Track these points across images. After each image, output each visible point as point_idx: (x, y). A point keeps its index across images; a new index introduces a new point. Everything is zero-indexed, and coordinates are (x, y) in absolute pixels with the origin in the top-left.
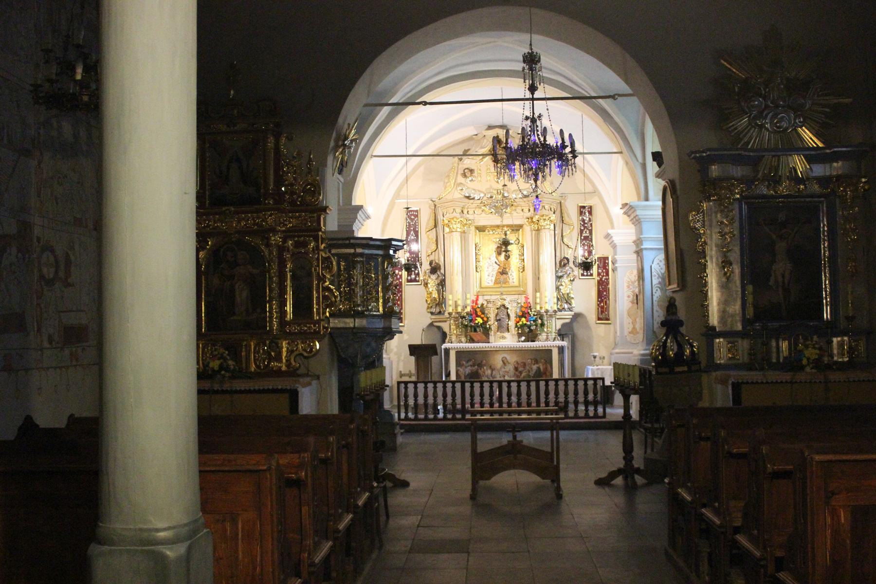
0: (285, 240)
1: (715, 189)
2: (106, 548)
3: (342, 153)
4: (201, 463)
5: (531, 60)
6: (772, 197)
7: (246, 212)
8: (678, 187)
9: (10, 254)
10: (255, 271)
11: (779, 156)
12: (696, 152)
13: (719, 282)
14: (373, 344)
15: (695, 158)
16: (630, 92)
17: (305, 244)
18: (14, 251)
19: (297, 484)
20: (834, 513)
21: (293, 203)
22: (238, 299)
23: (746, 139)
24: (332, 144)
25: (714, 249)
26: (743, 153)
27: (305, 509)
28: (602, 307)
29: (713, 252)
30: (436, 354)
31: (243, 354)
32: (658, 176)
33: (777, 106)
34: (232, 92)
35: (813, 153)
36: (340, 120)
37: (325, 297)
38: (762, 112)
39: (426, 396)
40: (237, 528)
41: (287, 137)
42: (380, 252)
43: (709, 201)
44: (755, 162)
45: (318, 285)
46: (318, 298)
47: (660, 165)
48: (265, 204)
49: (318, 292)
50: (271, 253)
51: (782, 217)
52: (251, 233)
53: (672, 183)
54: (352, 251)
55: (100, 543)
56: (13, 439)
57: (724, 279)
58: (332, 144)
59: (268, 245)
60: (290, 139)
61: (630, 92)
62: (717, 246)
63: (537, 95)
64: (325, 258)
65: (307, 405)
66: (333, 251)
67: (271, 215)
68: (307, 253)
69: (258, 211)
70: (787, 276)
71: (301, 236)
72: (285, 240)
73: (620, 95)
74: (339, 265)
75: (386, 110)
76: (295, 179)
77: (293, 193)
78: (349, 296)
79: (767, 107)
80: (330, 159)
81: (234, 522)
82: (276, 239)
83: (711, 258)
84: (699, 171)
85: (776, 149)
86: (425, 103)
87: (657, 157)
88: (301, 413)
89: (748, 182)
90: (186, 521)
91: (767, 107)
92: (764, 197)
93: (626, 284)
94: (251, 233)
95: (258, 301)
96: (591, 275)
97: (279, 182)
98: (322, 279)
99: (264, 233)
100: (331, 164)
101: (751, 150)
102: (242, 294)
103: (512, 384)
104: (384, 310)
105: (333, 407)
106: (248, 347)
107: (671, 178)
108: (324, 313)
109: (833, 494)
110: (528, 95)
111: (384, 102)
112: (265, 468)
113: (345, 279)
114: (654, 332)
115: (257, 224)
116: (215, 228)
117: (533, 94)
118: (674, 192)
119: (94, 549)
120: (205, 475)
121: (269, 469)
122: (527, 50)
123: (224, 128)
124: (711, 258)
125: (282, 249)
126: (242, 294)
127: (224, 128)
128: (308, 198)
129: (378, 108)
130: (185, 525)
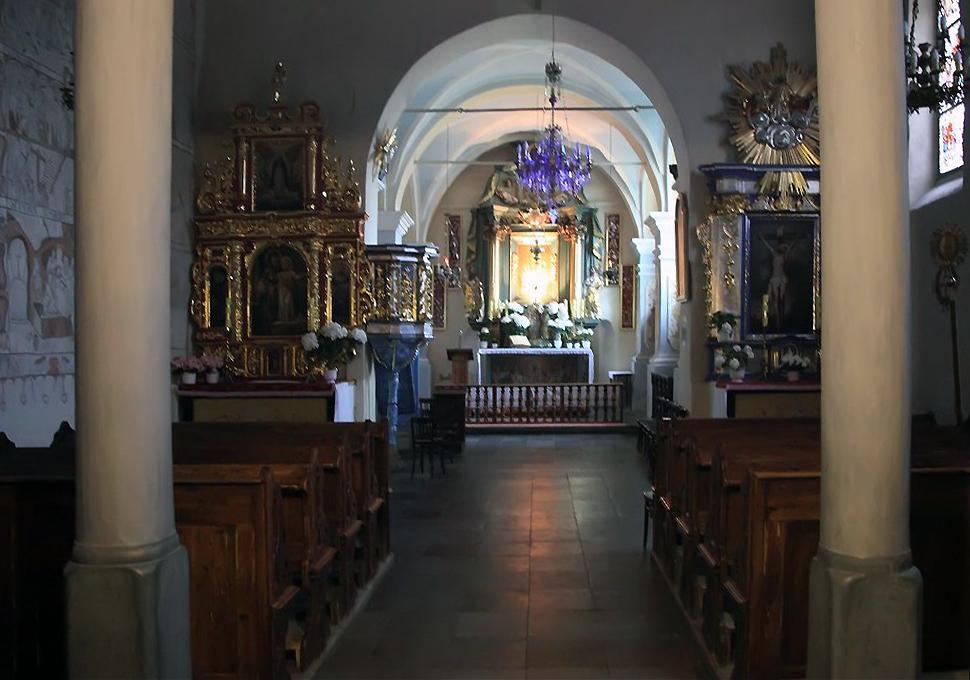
0: (325, 247)
1: (721, 203)
2: (82, 566)
3: (382, 159)
4: (176, 475)
5: (553, 71)
6: (773, 212)
7: (288, 218)
8: (688, 197)
9: (56, 257)
10: (297, 277)
11: (779, 172)
12: (708, 166)
13: (721, 293)
14: (407, 350)
15: (705, 172)
16: (651, 105)
17: (344, 251)
18: (59, 253)
19: (300, 494)
20: (772, 530)
21: (333, 209)
22: (281, 304)
23: (750, 155)
24: (372, 150)
25: (719, 262)
26: (747, 168)
27: (307, 520)
28: (626, 315)
29: (718, 265)
30: (472, 359)
31: (285, 358)
32: (674, 188)
33: (781, 122)
34: (277, 94)
35: (811, 170)
36: (380, 126)
37: (363, 304)
38: (766, 129)
39: (511, 400)
40: (234, 539)
41: (329, 142)
42: (415, 260)
43: (716, 214)
44: (758, 177)
45: (356, 290)
46: (356, 304)
47: (675, 177)
48: (307, 209)
49: (356, 298)
50: (312, 258)
51: (780, 232)
52: (294, 238)
53: (683, 196)
54: (389, 258)
55: (76, 561)
56: (48, 446)
57: (726, 292)
58: (372, 150)
59: (309, 251)
60: (331, 143)
61: (651, 105)
62: (722, 259)
63: (556, 105)
64: (362, 264)
65: (344, 413)
66: (370, 258)
67: (312, 221)
68: (345, 260)
69: (300, 217)
70: (783, 288)
71: (341, 242)
72: (325, 247)
73: (643, 107)
74: (376, 272)
75: (428, 116)
76: (336, 184)
77: (334, 199)
78: (385, 302)
79: (771, 123)
80: (370, 165)
81: (232, 532)
82: (317, 245)
83: (716, 269)
84: (708, 184)
85: (779, 166)
86: (461, 110)
87: (673, 169)
88: (335, 420)
89: (754, 197)
90: (157, 539)
91: (771, 123)
92: (766, 211)
93: (647, 294)
94: (294, 238)
95: (301, 306)
96: (618, 283)
97: (321, 186)
98: (359, 285)
99: (306, 239)
100: (371, 169)
101: (756, 165)
102: (285, 299)
103: (539, 389)
104: (418, 317)
105: (370, 414)
106: (289, 351)
107: (683, 191)
108: (361, 319)
109: (772, 509)
110: (550, 105)
111: (426, 108)
112: (259, 481)
113: (381, 284)
114: (668, 340)
115: (298, 229)
116: (260, 232)
117: (553, 105)
118: (685, 205)
119: (70, 566)
120: (182, 488)
121: (263, 482)
122: (549, 61)
123: (268, 130)
124: (716, 269)
125: (323, 255)
126: (285, 299)
127: (269, 131)
128: (347, 204)
129: (421, 114)
130: (158, 543)
